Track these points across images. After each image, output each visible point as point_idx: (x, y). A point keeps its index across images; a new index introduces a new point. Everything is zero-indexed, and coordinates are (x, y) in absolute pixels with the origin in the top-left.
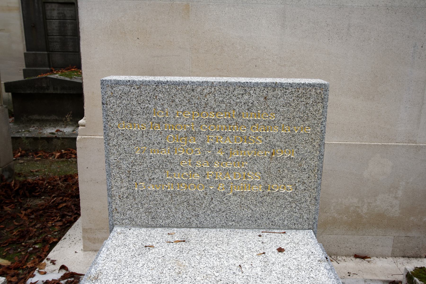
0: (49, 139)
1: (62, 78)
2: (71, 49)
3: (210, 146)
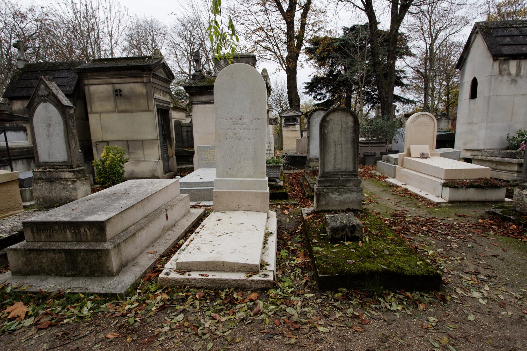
0: (185, 168)
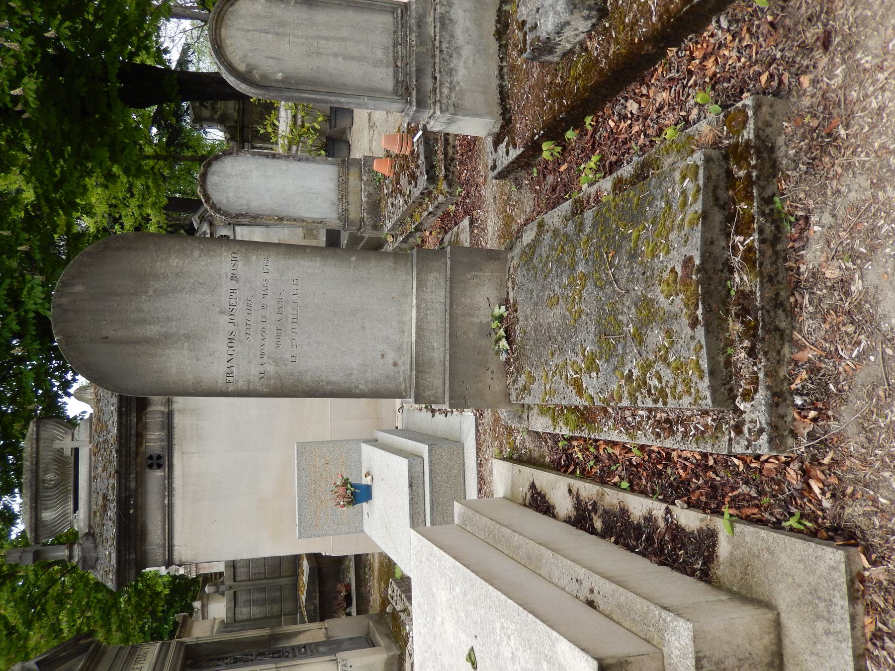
1: (305, 592)
2: (278, 594)
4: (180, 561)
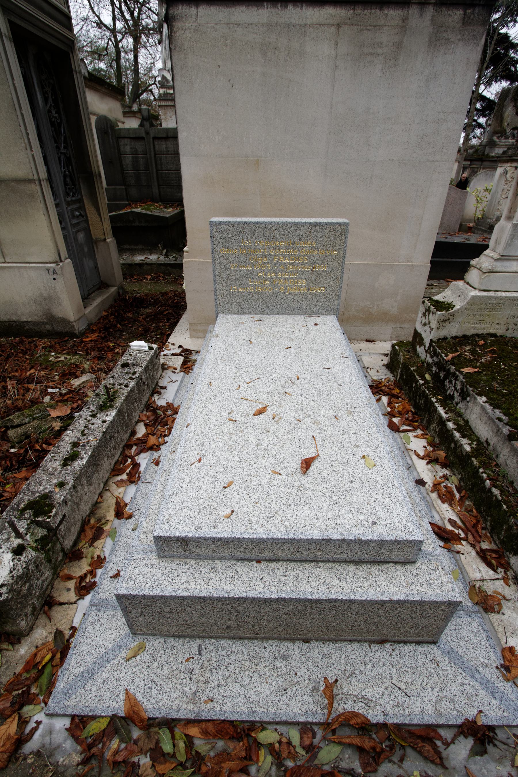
0: (140, 265)
1: (144, 211)
3: (276, 264)
4: (174, 18)
